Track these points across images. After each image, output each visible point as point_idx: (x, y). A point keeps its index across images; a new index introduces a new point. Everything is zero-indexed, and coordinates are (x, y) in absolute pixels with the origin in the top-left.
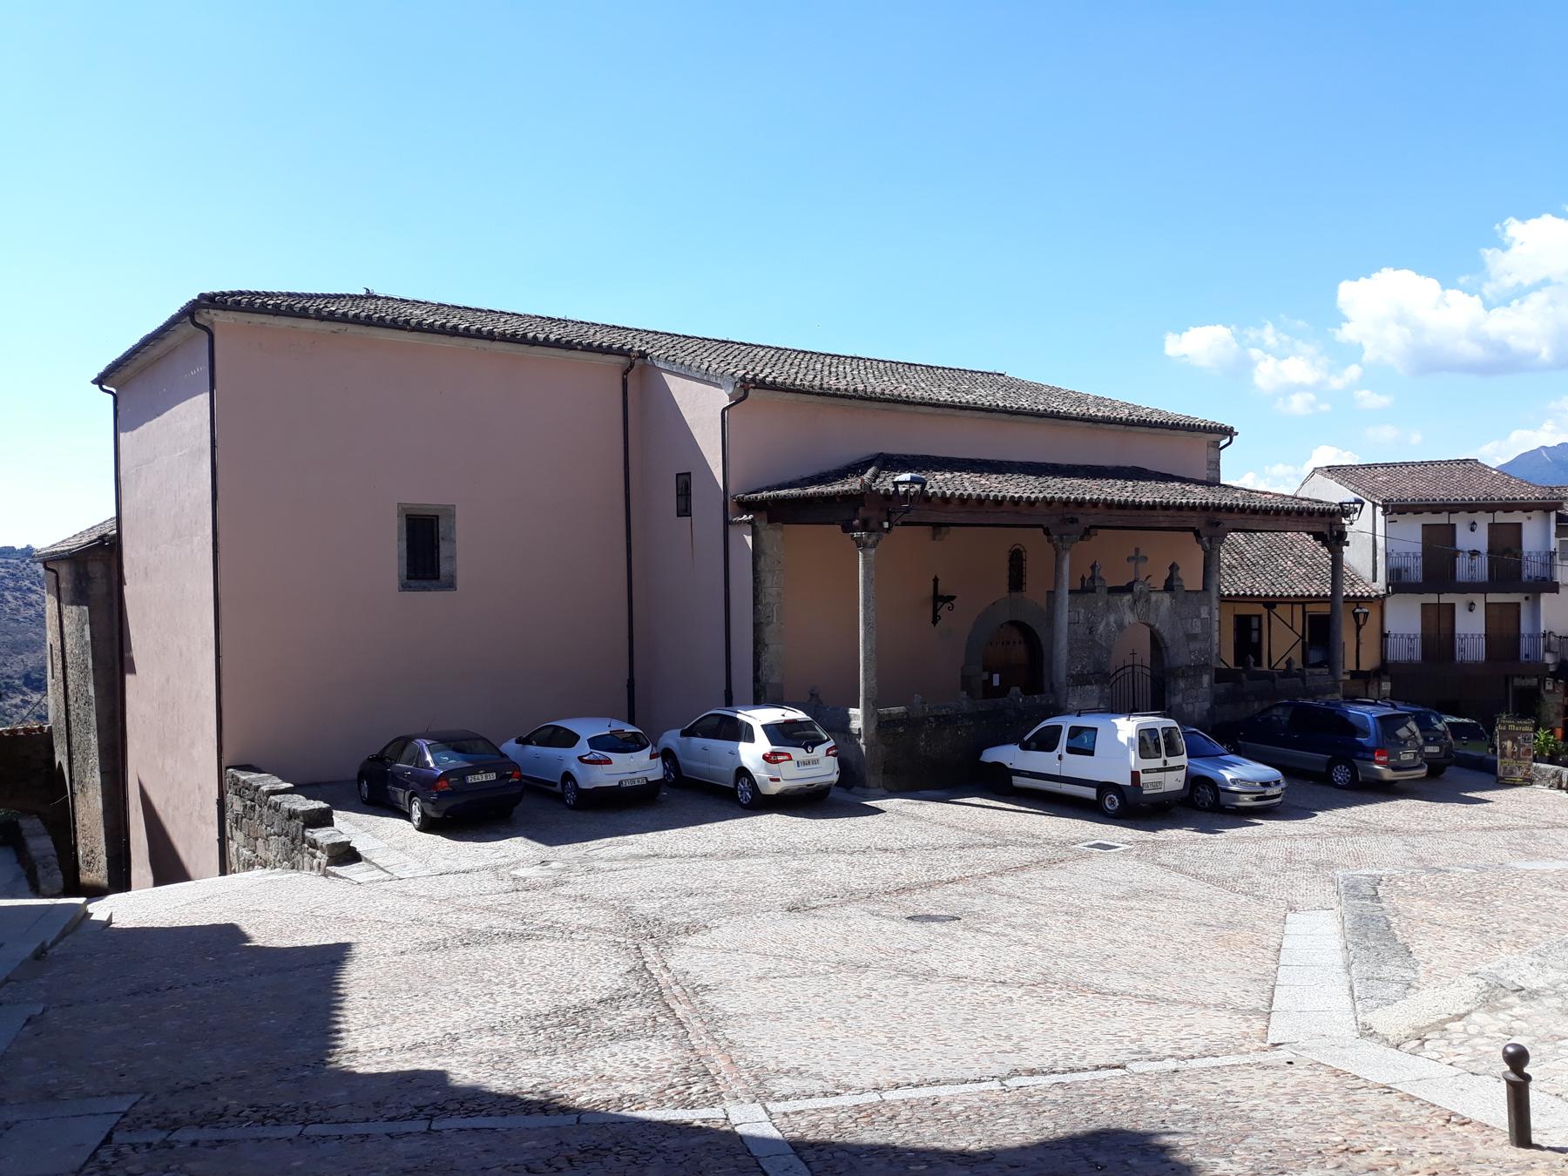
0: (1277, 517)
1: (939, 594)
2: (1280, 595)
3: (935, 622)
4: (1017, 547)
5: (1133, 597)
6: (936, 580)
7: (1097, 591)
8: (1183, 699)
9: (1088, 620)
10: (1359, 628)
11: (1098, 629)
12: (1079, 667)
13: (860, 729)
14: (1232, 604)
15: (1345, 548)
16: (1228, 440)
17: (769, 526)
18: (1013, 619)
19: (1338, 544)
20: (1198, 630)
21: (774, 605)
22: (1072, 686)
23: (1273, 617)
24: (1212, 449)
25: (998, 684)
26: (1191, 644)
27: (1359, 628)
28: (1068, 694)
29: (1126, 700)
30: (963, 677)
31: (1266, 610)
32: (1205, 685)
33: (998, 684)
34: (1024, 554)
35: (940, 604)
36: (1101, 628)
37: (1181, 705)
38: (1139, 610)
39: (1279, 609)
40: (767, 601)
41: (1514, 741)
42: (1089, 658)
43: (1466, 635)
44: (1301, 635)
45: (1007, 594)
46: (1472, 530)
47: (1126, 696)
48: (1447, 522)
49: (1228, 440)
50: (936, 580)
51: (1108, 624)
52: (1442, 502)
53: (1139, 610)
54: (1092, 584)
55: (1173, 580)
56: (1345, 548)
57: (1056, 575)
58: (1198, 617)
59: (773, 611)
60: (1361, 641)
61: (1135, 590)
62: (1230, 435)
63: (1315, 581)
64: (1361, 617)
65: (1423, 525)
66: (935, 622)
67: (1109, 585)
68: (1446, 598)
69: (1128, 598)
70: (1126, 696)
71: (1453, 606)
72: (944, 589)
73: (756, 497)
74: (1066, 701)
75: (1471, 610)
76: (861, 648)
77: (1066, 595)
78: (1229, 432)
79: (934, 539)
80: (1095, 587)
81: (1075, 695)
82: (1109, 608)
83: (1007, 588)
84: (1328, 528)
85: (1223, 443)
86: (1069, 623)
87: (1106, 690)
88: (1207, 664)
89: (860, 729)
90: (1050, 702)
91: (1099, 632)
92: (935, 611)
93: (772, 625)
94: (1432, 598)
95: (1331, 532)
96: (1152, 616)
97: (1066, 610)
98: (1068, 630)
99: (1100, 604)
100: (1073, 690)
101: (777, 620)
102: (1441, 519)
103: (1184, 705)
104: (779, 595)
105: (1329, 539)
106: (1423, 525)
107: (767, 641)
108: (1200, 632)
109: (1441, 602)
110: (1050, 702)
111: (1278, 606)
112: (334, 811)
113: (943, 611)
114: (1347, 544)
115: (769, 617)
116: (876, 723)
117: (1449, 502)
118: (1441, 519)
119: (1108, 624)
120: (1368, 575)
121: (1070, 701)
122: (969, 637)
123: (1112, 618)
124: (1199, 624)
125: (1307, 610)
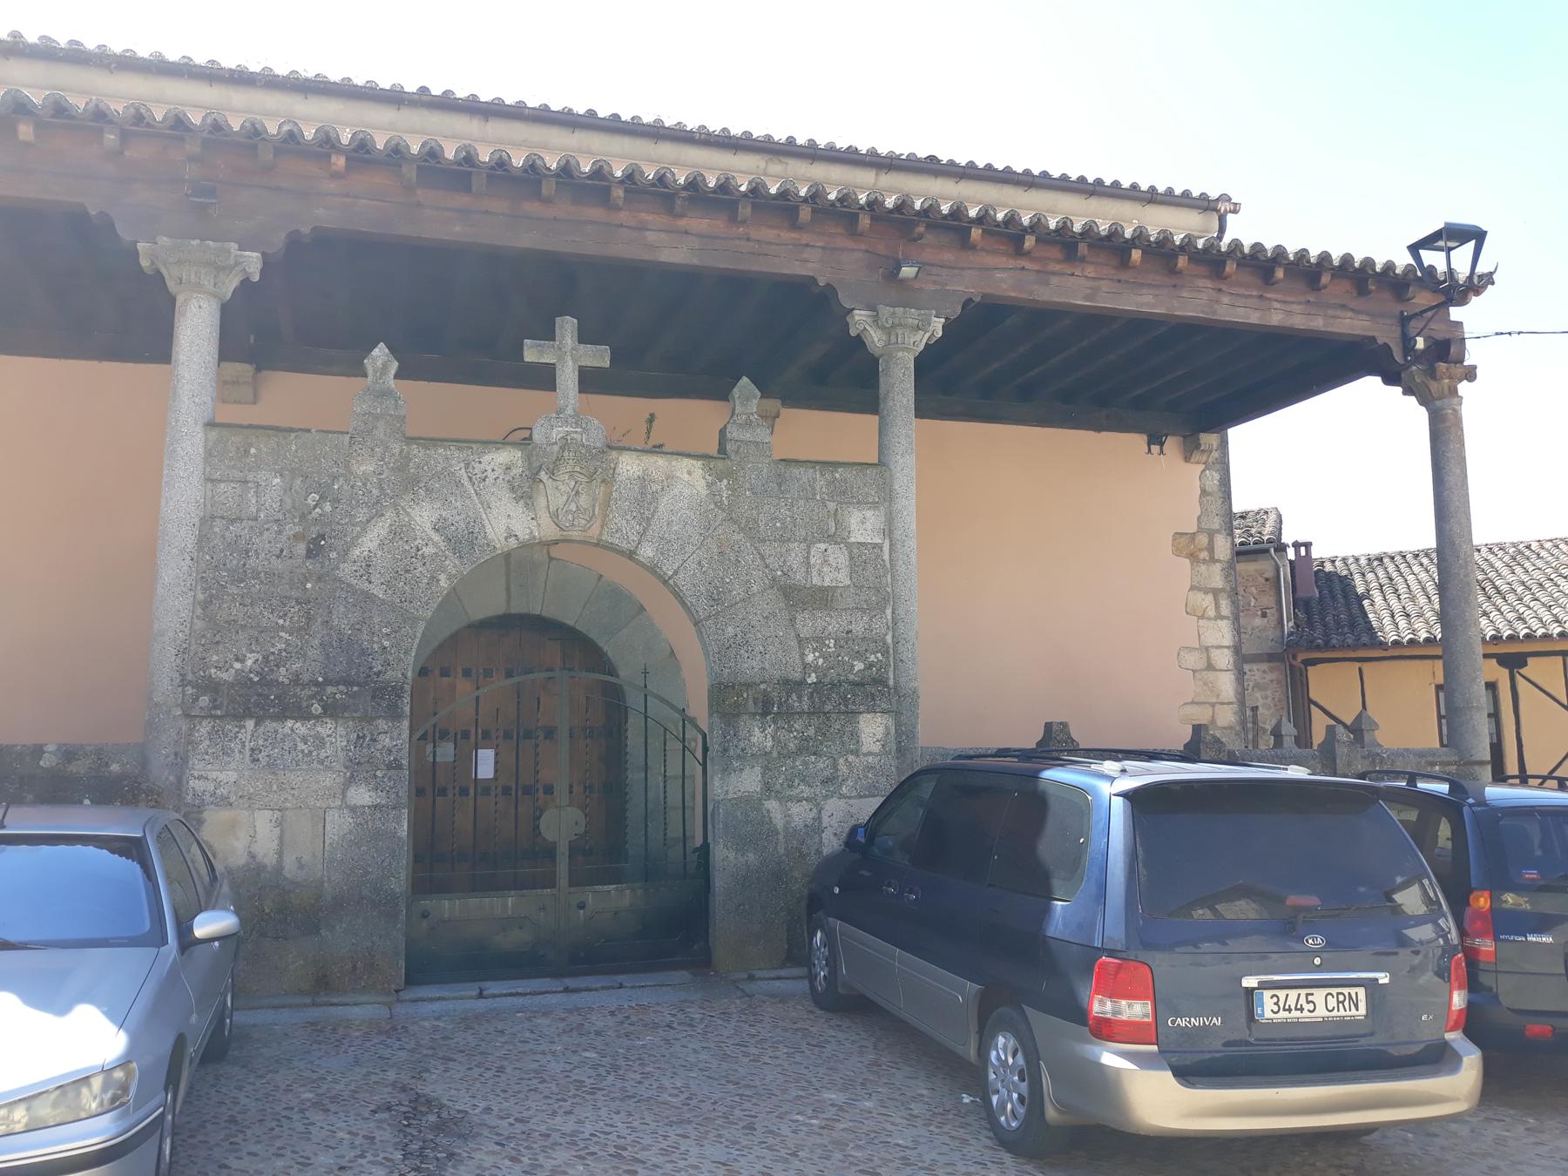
2: (1527, 636)
8: (768, 788)
11: (353, 543)
14: (1429, 662)
15: (1464, 388)
23: (1522, 684)
25: (490, 775)
31: (1505, 672)
33: (490, 775)
36: (370, 542)
39: (1534, 668)
41: (846, 697)
56: (1464, 388)
76: (1471, 858)
84: (1396, 332)
95: (1407, 343)
105: (1398, 357)
108: (843, 578)
111: (1530, 661)
114: (1470, 374)
119: (399, 532)
121: (197, 766)
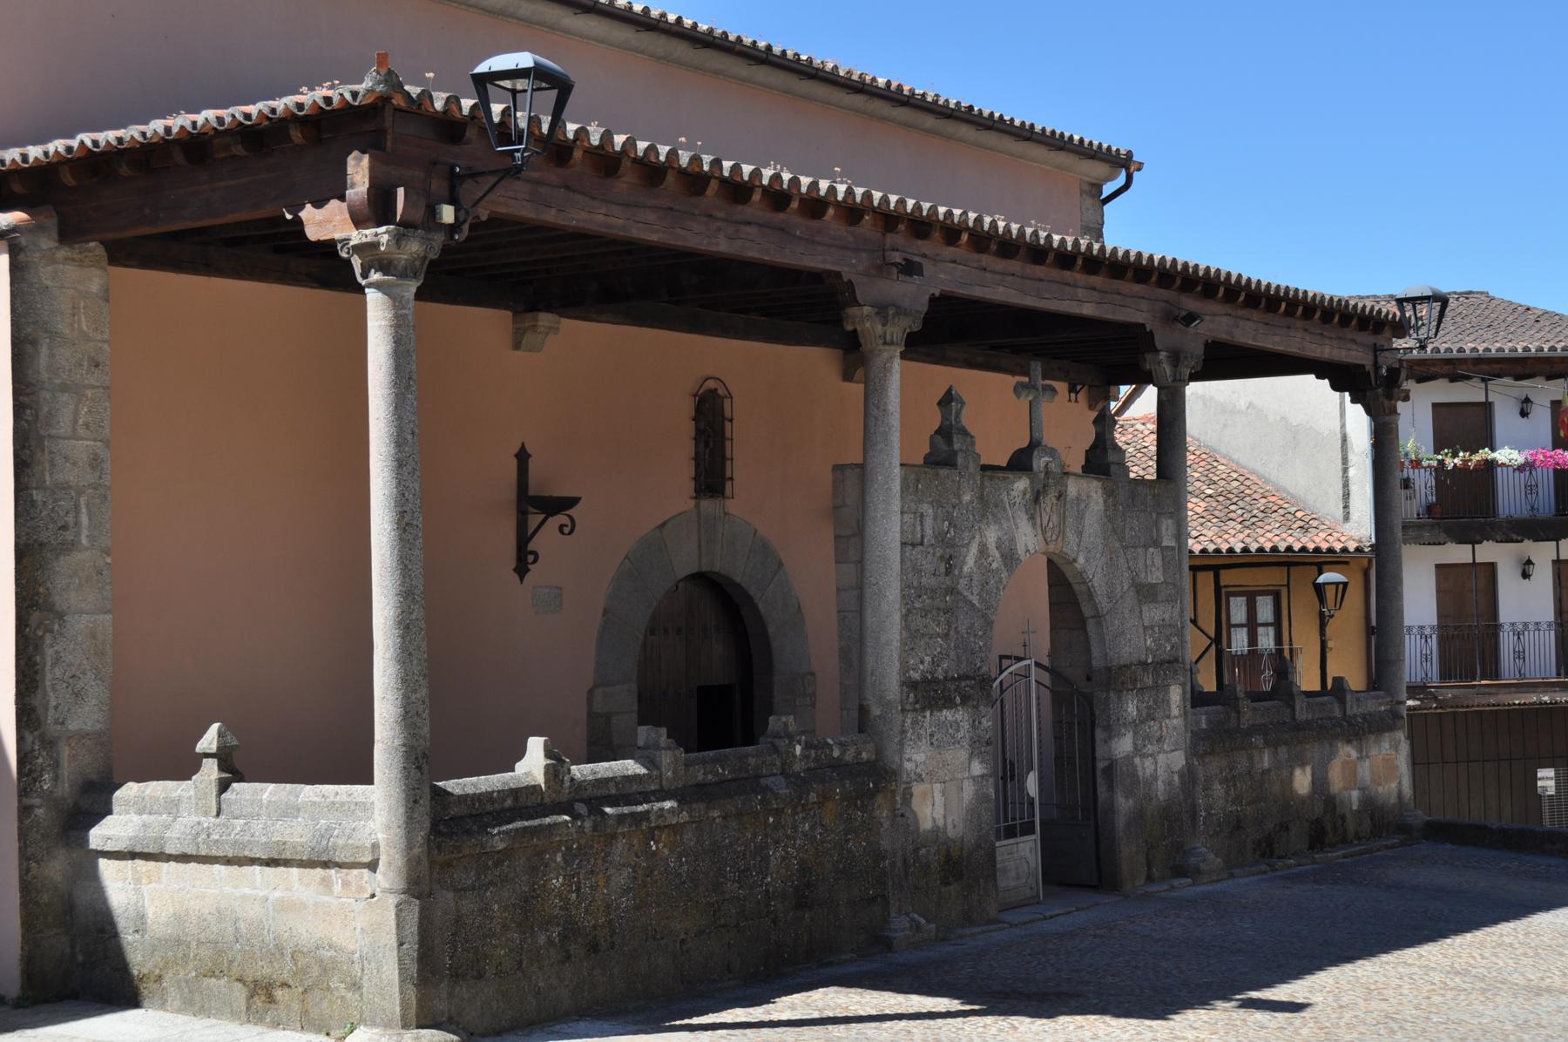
0: (1289, 320)
1: (531, 493)
3: (522, 569)
4: (711, 384)
5: (1032, 483)
6: (523, 457)
7: (960, 461)
9: (941, 537)
10: (1323, 622)
11: (964, 563)
12: (928, 659)
13: (375, 846)
15: (1401, 406)
16: (1121, 180)
17: (63, 253)
18: (704, 569)
19: (1390, 397)
20: (1156, 576)
21: (80, 493)
22: (915, 710)
24: (1088, 201)
26: (1145, 608)
27: (1323, 622)
28: (904, 732)
29: (1413, 661)
30: (591, 715)
32: (1175, 711)
34: (727, 402)
35: (534, 519)
36: (970, 562)
37: (1129, 759)
38: (1045, 519)
40: (60, 477)
42: (946, 636)
43: (1526, 625)
44: (1213, 635)
45: (692, 503)
46: (1524, 414)
47: (1413, 656)
48: (1484, 400)
49: (1121, 180)
50: (523, 457)
51: (983, 551)
52: (1474, 355)
53: (1045, 519)
54: (944, 447)
55: (1105, 450)
57: (866, 414)
58: (1156, 543)
59: (77, 507)
60: (1330, 644)
61: (1035, 467)
62: (1127, 169)
63: (1231, 523)
64: (1330, 593)
65: (1435, 405)
66: (522, 569)
67: (984, 461)
68: (1488, 551)
69: (1021, 484)
70: (1413, 656)
71: (1491, 568)
72: (548, 478)
73: (25, 157)
74: (901, 751)
75: (1525, 575)
77: (897, 470)
78: (1123, 163)
79: (517, 345)
80: (955, 453)
81: (919, 738)
82: (987, 508)
83: (690, 487)
85: (1108, 190)
86: (903, 544)
87: (986, 723)
88: (1176, 660)
89: (375, 846)
90: (864, 755)
91: (965, 569)
92: (523, 540)
93: (78, 556)
94: (1459, 554)
95: (1377, 367)
96: (1071, 537)
97: (896, 505)
98: (902, 561)
99: (967, 498)
100: (915, 722)
101: (91, 538)
102: (1467, 393)
103: (1137, 761)
104: (95, 462)
106: (1435, 405)
107: (58, 601)
109: (1477, 561)
110: (864, 755)
112: (1401, 735)
113: (547, 539)
115: (64, 528)
116: (427, 825)
117: (1488, 355)
118: (1467, 393)
119: (983, 551)
120: (1335, 509)
122: (605, 612)
123: (992, 535)
124: (1158, 560)
125: (1222, 583)
